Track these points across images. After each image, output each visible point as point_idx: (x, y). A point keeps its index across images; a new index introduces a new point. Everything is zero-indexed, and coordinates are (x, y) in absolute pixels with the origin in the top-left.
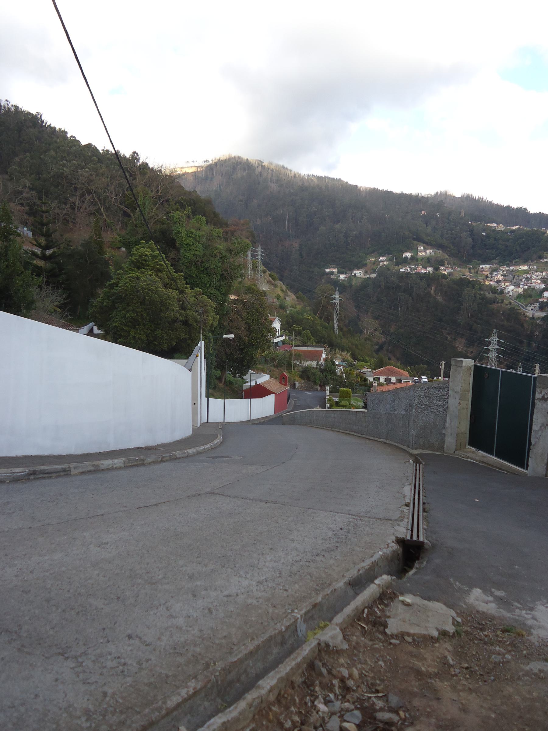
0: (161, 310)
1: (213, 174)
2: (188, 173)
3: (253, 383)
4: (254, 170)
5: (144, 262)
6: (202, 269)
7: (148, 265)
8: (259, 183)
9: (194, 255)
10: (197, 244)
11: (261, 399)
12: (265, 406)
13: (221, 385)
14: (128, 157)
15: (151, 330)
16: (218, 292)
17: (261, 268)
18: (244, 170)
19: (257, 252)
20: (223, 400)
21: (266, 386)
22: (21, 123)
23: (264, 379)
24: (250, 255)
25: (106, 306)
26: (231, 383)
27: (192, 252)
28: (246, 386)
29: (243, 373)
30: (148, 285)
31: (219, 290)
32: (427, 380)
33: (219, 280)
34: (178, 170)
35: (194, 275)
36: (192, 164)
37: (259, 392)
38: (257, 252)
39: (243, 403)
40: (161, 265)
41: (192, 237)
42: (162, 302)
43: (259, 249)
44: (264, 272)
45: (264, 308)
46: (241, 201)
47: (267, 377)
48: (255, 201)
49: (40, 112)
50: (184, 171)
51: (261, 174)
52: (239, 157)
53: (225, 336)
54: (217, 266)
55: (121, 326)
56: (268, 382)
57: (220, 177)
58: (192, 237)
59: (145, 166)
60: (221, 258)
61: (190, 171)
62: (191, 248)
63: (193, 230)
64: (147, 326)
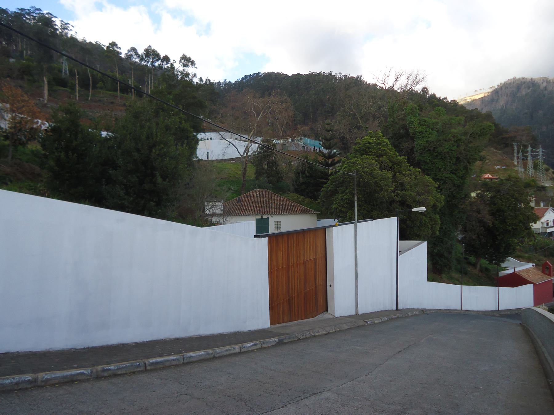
0: (375, 190)
1: (498, 96)
2: (476, 99)
3: (511, 271)
4: (539, 86)
5: (367, 149)
6: (435, 154)
7: (371, 152)
8: (544, 96)
9: (427, 141)
10: (430, 131)
11: (514, 288)
12: (521, 297)
13: (476, 271)
14: (419, 92)
15: (368, 211)
16: (454, 176)
17: (543, 166)
18: (529, 87)
19: (538, 152)
20: (460, 286)
21: (523, 274)
22: (348, 85)
23: (523, 267)
24: (530, 156)
25: (330, 190)
26: (487, 270)
27: (425, 139)
28: (502, 273)
29: (502, 259)
30: (363, 168)
31: (456, 174)
32: (70, 152)
33: (455, 164)
34: (468, 98)
35: (428, 161)
36: (479, 92)
37: (515, 281)
38: (538, 152)
39: (504, 291)
40: (384, 150)
41: (425, 125)
42: (376, 183)
43: (540, 150)
44: (547, 170)
45: (522, 194)
46: (526, 113)
47: (530, 266)
48: (540, 112)
49: (360, 74)
50: (473, 98)
51: (546, 88)
52: (523, 78)
53: (414, 210)
54: (452, 150)
55: (340, 208)
56: (527, 271)
57: (505, 97)
58: (425, 125)
59: (433, 96)
60: (456, 141)
61: (477, 97)
62: (423, 135)
63: (426, 119)
64: (363, 207)
